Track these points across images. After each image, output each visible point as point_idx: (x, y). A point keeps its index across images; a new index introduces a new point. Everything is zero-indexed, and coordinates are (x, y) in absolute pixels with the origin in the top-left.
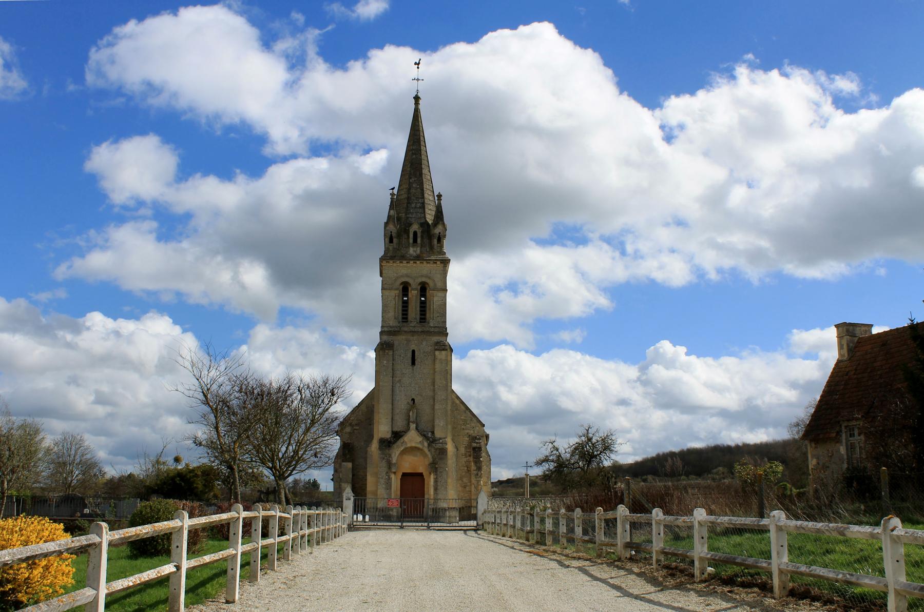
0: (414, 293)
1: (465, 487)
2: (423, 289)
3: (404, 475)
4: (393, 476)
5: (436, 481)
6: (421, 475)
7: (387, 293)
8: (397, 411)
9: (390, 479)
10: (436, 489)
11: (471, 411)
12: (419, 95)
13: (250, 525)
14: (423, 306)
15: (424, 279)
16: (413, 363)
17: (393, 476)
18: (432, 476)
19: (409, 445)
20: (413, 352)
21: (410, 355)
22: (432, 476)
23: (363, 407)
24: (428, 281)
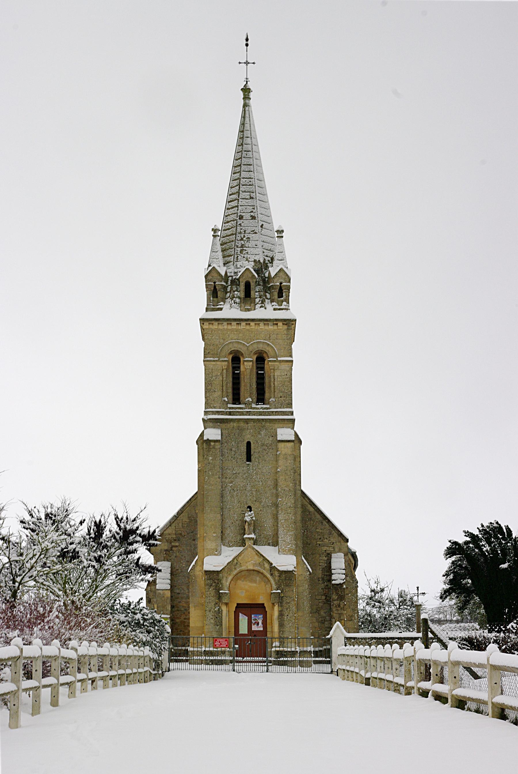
0: (247, 366)
1: (323, 622)
2: (261, 360)
3: (238, 604)
4: (224, 608)
5: (281, 614)
6: (263, 604)
7: (211, 365)
8: (228, 522)
9: (220, 612)
10: (281, 625)
11: (329, 521)
12: (250, 85)
13: (426, 676)
14: (261, 380)
15: (261, 347)
16: (249, 459)
17: (224, 608)
18: (276, 608)
19: (243, 568)
20: (249, 444)
21: (244, 448)
22: (276, 608)
23: (184, 518)
24: (267, 349)
